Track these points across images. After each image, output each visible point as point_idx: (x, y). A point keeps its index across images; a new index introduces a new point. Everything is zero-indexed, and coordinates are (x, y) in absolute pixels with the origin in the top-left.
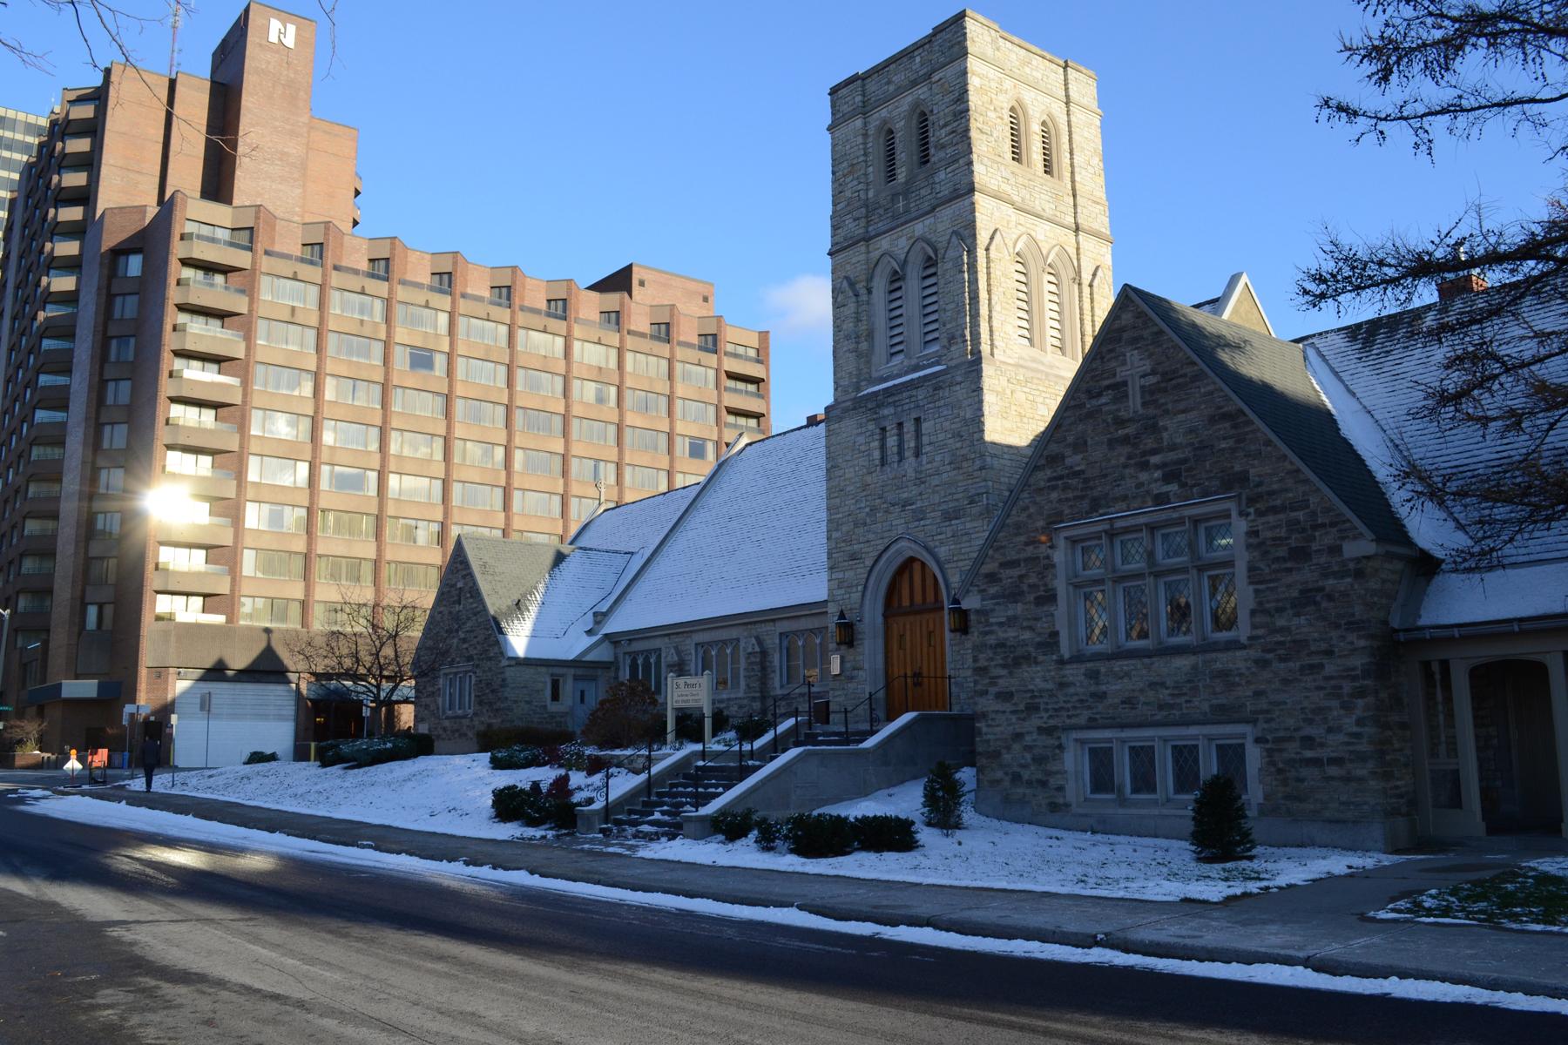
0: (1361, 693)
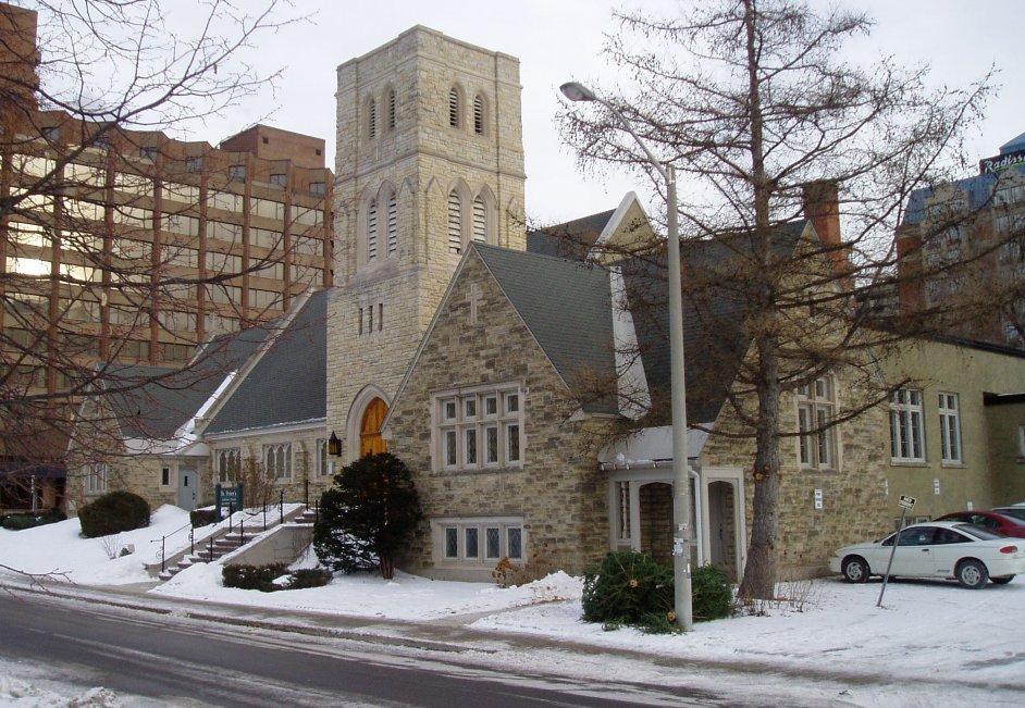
0: (574, 501)
